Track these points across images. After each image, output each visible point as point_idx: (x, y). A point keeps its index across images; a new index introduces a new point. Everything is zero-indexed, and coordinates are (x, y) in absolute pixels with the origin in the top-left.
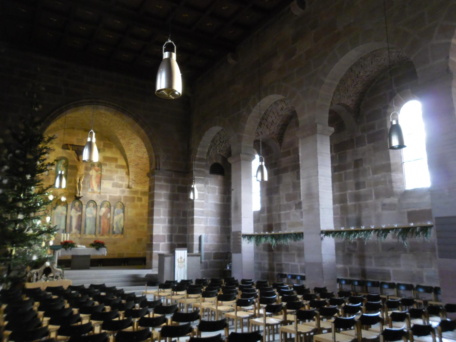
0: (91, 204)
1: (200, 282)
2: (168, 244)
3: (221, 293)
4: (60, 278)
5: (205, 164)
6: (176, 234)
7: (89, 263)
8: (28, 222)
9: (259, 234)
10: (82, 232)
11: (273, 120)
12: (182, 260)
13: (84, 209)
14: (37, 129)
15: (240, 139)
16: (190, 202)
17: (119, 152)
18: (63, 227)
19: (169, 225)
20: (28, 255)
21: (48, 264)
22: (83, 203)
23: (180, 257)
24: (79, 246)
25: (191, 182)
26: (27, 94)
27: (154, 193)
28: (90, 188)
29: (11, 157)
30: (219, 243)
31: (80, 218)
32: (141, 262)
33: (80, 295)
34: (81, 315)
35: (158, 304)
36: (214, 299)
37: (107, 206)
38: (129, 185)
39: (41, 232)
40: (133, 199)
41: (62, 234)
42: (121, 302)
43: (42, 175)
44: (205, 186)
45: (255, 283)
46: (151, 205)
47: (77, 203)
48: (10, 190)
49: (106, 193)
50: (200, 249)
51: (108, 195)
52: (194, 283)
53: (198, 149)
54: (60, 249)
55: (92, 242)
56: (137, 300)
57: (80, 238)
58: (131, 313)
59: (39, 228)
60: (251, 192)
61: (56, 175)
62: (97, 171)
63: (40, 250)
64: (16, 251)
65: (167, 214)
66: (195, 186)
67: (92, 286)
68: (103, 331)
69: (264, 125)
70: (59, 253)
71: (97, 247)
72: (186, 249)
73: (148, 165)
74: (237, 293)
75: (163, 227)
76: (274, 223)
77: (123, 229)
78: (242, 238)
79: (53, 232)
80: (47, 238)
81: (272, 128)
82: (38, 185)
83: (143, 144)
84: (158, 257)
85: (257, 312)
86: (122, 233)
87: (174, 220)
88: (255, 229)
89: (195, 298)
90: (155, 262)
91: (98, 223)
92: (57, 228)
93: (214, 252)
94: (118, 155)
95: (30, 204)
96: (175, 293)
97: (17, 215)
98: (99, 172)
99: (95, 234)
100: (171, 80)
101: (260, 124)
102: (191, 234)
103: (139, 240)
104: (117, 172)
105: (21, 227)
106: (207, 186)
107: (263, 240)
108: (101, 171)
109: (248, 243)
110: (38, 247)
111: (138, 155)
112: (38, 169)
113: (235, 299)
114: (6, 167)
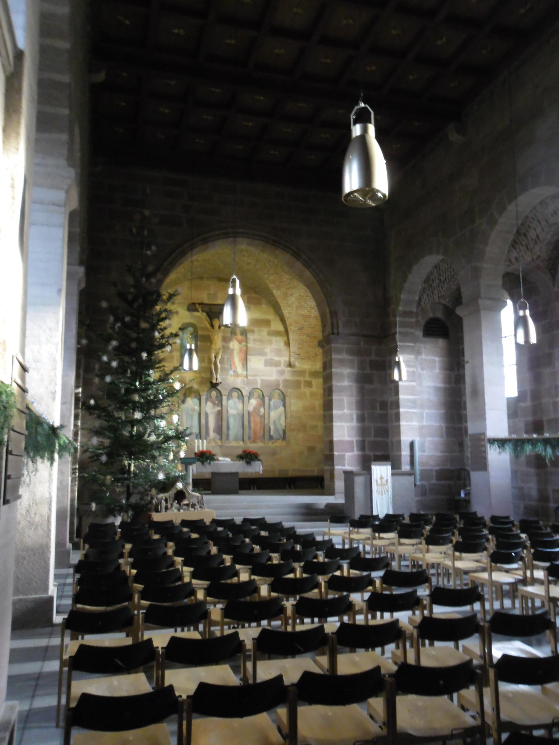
0: (235, 394)
1: (418, 520)
2: (359, 456)
3: (456, 538)
4: (198, 506)
5: (414, 320)
6: (372, 438)
7: (237, 484)
8: (148, 423)
9: (520, 437)
10: (224, 437)
11: (538, 236)
12: (384, 481)
13: (224, 402)
14: (151, 283)
15: (476, 273)
16: (392, 386)
17: (272, 310)
18: (195, 430)
19: (359, 425)
20: (152, 472)
21: (180, 485)
22: (223, 392)
23: (379, 476)
24: (221, 458)
25: (394, 351)
26: (134, 230)
27: (331, 372)
28: (231, 369)
29: (119, 327)
30: (446, 454)
31: (220, 415)
32: (317, 483)
33: (230, 535)
34: (238, 567)
35: (292, 532)
36: (448, 548)
37: (259, 397)
38: (290, 362)
39: (168, 439)
40: (297, 385)
41: (196, 441)
42: (293, 548)
43: (162, 352)
44: (416, 359)
45: (517, 523)
46: (328, 391)
47: (214, 393)
48: (120, 376)
49: (256, 376)
50: (412, 463)
51: (259, 379)
52: (407, 521)
53: (402, 296)
54: (194, 463)
55: (240, 452)
56: (320, 545)
57: (221, 447)
58: (314, 568)
59: (164, 432)
60: (501, 365)
61: (183, 350)
62: (240, 342)
63: (166, 465)
64: (135, 466)
65: (354, 407)
66: (401, 358)
67: (245, 520)
68: (274, 594)
69: (522, 244)
70: (194, 469)
71: (248, 460)
72: (390, 463)
73: (319, 327)
74: (488, 540)
75: (348, 427)
76: (545, 418)
77: (284, 432)
78: (488, 445)
79: (183, 437)
80: (176, 447)
81: (537, 248)
82: (157, 368)
83: (310, 294)
84: (343, 477)
85: (528, 574)
86: (284, 438)
87: (366, 415)
88: (512, 429)
89: (413, 545)
90: (339, 484)
91: (246, 423)
92: (188, 432)
93: (437, 468)
94: (271, 316)
95: (149, 396)
96: (377, 535)
97: (133, 413)
98: (244, 343)
99: (243, 440)
100: (369, 172)
101: (514, 244)
102: (395, 439)
103: (311, 449)
104: (271, 342)
105: (140, 431)
106: (419, 357)
107: (528, 449)
108: (247, 342)
109: (500, 453)
110: (165, 460)
111: (302, 313)
112: (156, 343)
113: (485, 549)
114: (114, 343)
